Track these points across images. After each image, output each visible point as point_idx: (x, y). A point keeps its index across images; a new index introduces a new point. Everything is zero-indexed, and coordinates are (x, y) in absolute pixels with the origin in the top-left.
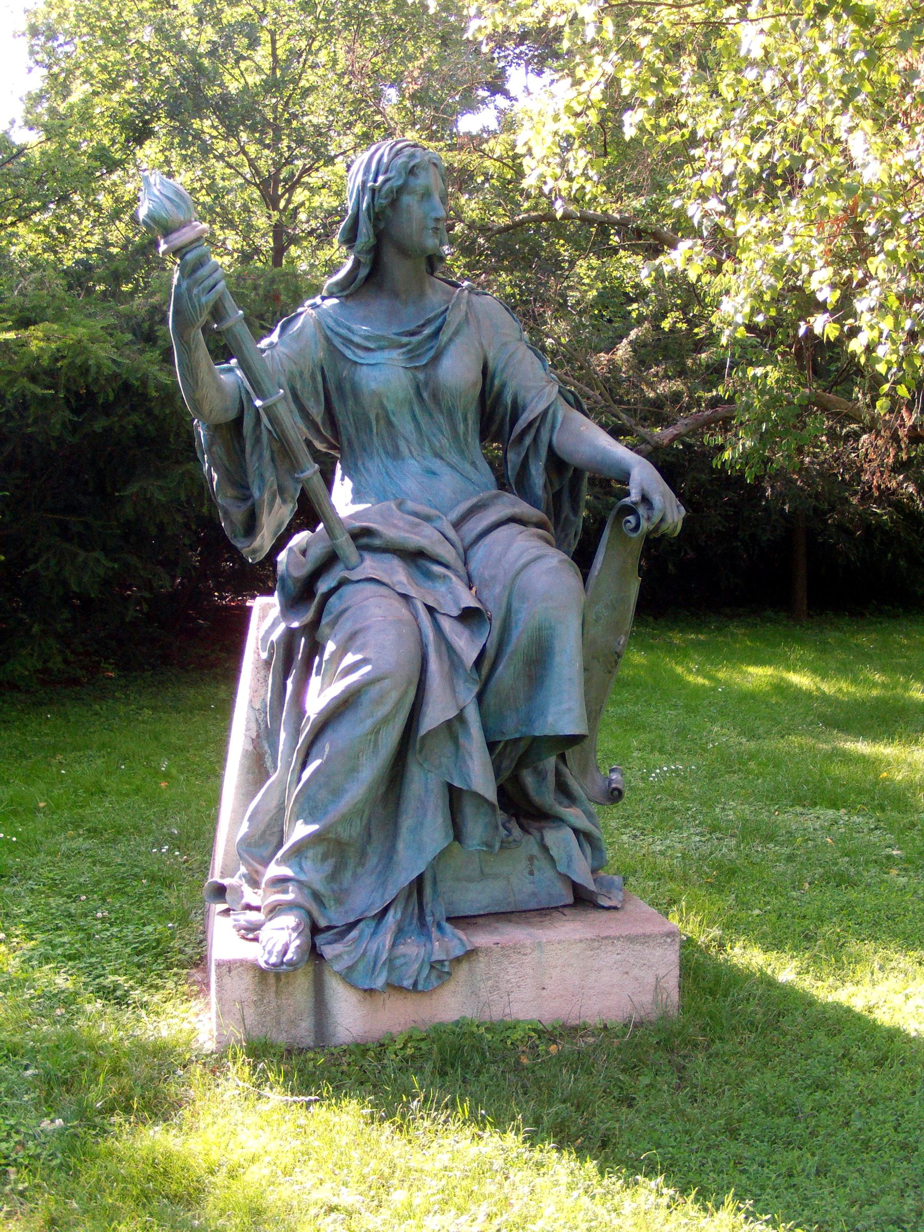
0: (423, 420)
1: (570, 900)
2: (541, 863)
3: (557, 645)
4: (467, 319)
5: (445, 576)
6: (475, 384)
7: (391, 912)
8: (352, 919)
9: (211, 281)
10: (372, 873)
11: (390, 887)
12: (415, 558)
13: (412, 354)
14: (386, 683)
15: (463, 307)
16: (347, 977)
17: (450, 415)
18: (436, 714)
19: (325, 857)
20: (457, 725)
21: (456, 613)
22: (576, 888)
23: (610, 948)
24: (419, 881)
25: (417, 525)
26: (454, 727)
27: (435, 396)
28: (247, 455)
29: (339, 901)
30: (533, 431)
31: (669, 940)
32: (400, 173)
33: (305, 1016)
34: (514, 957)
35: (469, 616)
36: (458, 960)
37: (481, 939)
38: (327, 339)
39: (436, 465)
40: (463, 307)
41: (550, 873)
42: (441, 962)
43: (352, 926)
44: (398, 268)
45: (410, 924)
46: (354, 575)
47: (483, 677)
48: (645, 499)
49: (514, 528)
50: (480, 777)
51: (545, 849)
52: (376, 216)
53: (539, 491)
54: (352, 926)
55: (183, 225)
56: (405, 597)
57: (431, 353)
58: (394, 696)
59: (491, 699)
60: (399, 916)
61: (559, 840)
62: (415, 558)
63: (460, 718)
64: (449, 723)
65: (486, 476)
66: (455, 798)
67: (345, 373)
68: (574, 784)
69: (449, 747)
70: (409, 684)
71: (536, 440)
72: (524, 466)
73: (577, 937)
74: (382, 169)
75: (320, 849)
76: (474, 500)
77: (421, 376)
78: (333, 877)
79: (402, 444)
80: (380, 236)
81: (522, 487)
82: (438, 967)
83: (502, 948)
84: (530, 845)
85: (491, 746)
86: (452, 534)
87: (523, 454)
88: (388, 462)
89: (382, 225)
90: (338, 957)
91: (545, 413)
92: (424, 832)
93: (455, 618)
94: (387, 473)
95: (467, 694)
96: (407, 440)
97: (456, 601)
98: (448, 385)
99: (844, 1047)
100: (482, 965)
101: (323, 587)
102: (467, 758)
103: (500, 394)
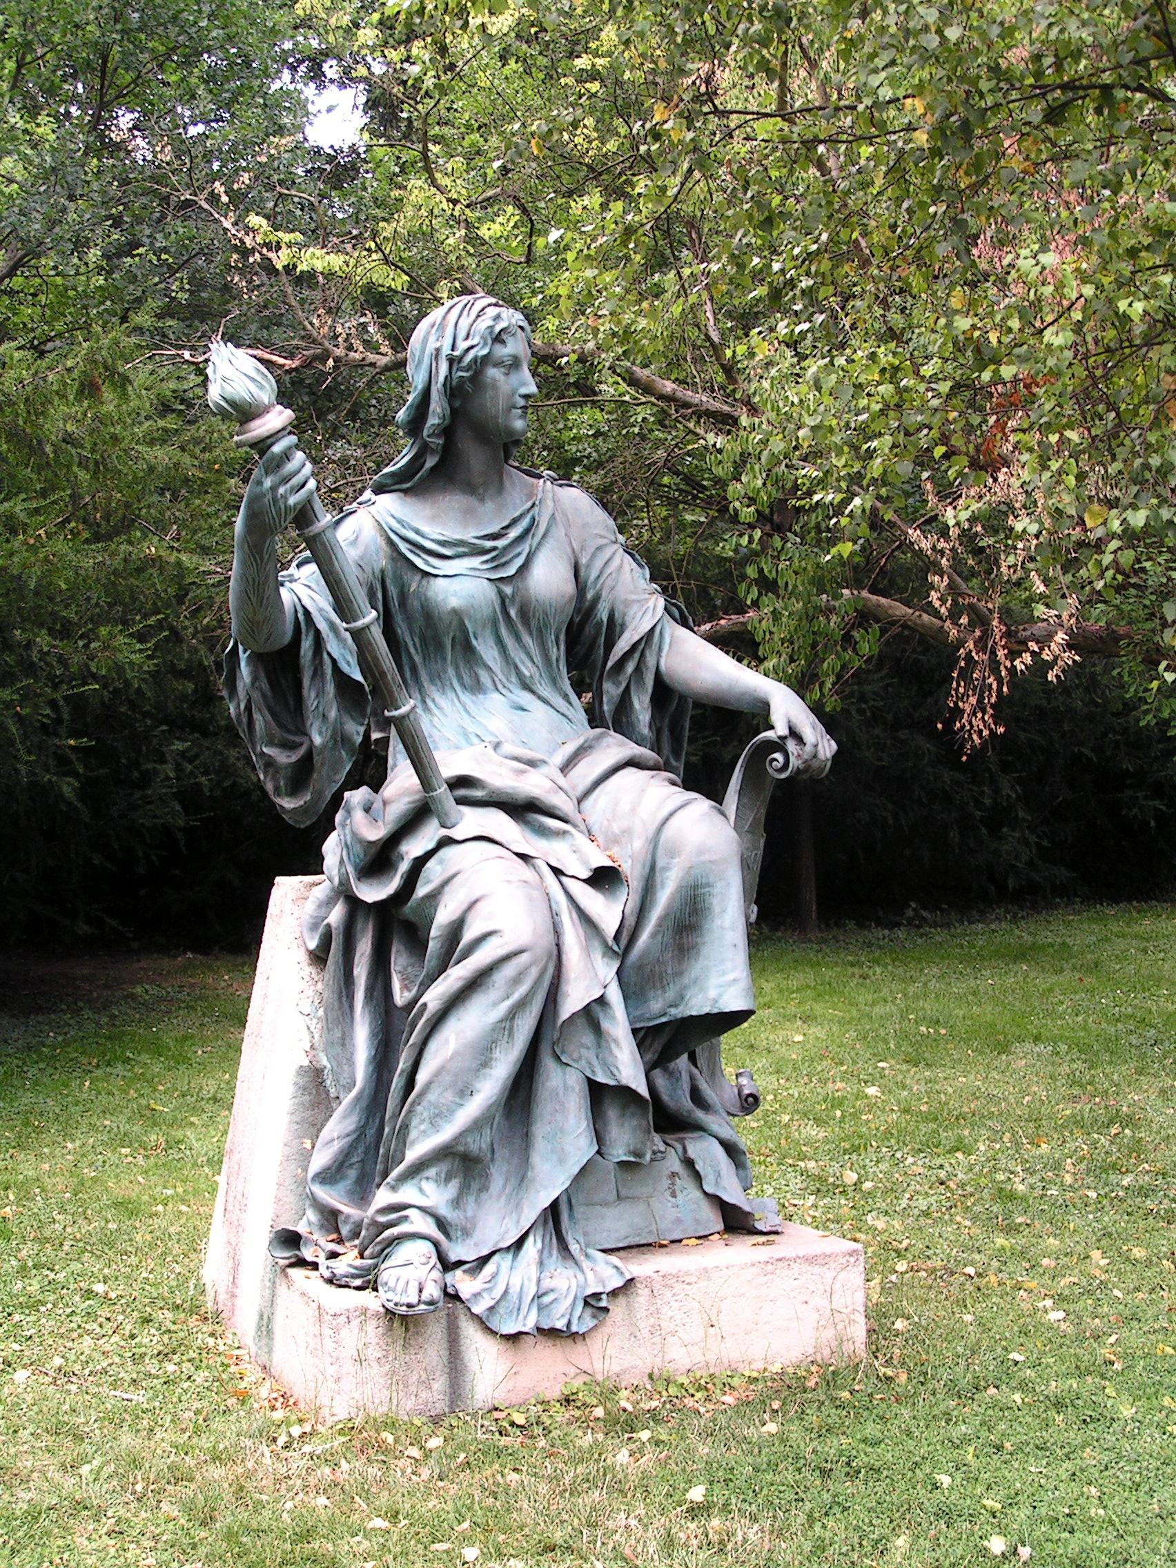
1: (720, 1226)
3: (715, 902)
5: (565, 832)
6: (571, 599)
7: (531, 1239)
8: (485, 1252)
9: (296, 481)
10: (500, 1196)
11: (526, 1210)
12: (523, 809)
13: (498, 559)
14: (524, 958)
15: (550, 503)
18: (573, 1000)
19: (448, 1179)
20: (596, 1008)
21: (585, 874)
23: (786, 1272)
24: (554, 1207)
25: (523, 772)
26: (592, 1014)
27: (524, 614)
28: (305, 692)
29: (466, 1233)
30: (637, 655)
31: (852, 1260)
32: (483, 338)
33: (438, 1373)
34: (678, 1287)
35: (604, 878)
36: (614, 1293)
37: (640, 1267)
38: (391, 543)
39: (525, 698)
40: (550, 503)
41: (689, 1194)
42: (597, 1296)
43: (484, 1260)
44: (475, 457)
45: (551, 1255)
46: (457, 833)
47: (622, 947)
48: (794, 734)
49: (630, 771)
51: (689, 1163)
52: (454, 391)
53: (646, 731)
54: (484, 1260)
56: (523, 857)
57: (519, 562)
60: (539, 1244)
61: (706, 1152)
62: (523, 809)
63: (602, 1001)
64: (587, 1009)
66: (598, 1094)
67: (413, 587)
69: (588, 1038)
70: (550, 957)
71: (638, 670)
72: (624, 703)
74: (462, 334)
75: (444, 1167)
76: (570, 748)
77: (508, 590)
78: (456, 1203)
79: (484, 677)
81: (621, 722)
82: (593, 1303)
83: (664, 1276)
85: (635, 1032)
87: (624, 685)
88: (466, 698)
89: (457, 404)
90: (477, 1295)
91: (652, 630)
92: (565, 1141)
93: (585, 881)
94: (466, 711)
95: (607, 970)
96: (489, 669)
98: (541, 598)
100: (641, 1299)
101: (413, 848)
102: (613, 1045)
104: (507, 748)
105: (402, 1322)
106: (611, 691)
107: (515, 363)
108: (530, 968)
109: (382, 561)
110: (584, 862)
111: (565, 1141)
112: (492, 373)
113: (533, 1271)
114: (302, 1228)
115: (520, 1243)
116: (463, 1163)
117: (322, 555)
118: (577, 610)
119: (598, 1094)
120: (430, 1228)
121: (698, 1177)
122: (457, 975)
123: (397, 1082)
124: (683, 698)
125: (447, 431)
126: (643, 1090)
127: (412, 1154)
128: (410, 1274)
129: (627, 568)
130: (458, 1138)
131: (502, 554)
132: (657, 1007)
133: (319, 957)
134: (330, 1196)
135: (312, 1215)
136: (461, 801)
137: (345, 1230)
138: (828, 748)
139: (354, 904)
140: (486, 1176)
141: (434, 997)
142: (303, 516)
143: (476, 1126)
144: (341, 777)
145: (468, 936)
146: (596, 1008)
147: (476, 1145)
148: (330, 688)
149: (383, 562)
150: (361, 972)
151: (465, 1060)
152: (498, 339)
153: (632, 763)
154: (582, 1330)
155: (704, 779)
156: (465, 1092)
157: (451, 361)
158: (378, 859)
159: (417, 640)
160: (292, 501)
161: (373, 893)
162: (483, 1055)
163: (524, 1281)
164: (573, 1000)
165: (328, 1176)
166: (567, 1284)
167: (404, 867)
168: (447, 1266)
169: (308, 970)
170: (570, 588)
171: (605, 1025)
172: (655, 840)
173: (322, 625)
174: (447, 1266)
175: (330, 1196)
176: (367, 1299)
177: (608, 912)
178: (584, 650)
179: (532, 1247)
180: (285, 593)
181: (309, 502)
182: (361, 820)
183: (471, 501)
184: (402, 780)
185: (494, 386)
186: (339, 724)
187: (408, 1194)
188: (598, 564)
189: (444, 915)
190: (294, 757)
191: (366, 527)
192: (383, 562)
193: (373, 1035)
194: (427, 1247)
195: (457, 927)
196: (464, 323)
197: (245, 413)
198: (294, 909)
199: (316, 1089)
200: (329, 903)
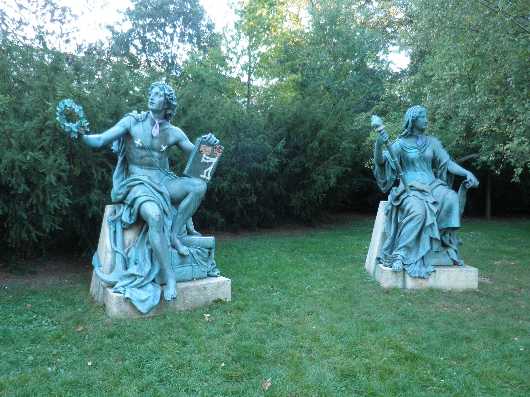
0: (421, 163)
2: (447, 255)
4: (430, 143)
12: (422, 191)
16: (409, 275)
17: (427, 162)
18: (428, 223)
20: (432, 225)
21: (432, 202)
22: (454, 261)
24: (423, 257)
29: (408, 260)
35: (435, 203)
37: (437, 269)
39: (424, 173)
41: (449, 258)
44: (416, 133)
46: (410, 195)
48: (471, 180)
51: (448, 252)
52: (413, 121)
54: (410, 265)
55: (380, 126)
58: (421, 218)
59: (439, 220)
62: (422, 191)
63: (433, 224)
65: (433, 176)
66: (431, 239)
68: (452, 240)
69: (430, 230)
71: (444, 169)
72: (441, 174)
73: (307, 383)
76: (431, 182)
77: (421, 155)
78: (406, 255)
81: (441, 177)
85: (439, 229)
88: (413, 172)
91: (446, 163)
92: (425, 246)
95: (435, 219)
97: (431, 200)
99: (464, 379)
101: (402, 197)
104: (420, 181)
105: (395, 272)
107: (424, 117)
108: (420, 218)
109: (400, 150)
110: (431, 200)
111: (425, 246)
112: (420, 119)
113: (418, 267)
114: (381, 257)
115: (416, 262)
116: (407, 248)
117: (389, 148)
118: (434, 158)
119: (431, 239)
121: (449, 255)
122: (408, 218)
123: (398, 235)
124: (452, 174)
125: (412, 128)
126: (439, 239)
127: (399, 246)
128: (398, 265)
130: (407, 244)
131: (422, 148)
132: (443, 226)
133: (387, 214)
134: (385, 252)
135: (383, 256)
136: (411, 190)
137: (388, 258)
138: (477, 183)
139: (393, 206)
140: (412, 251)
141: (404, 221)
142: (386, 143)
143: (410, 242)
144: (392, 185)
145: (411, 211)
146: (432, 225)
147: (411, 245)
148: (390, 170)
150: (393, 217)
151: (409, 233)
152: (421, 113)
153: (442, 184)
155: (455, 188)
156: (408, 237)
157: (413, 117)
158: (397, 198)
159: (405, 162)
160: (384, 140)
161: (396, 204)
162: (412, 231)
163: (415, 269)
164: (428, 223)
165: (386, 249)
166: (424, 270)
167: (401, 200)
168: (404, 265)
169: (385, 216)
170: (432, 155)
171: (434, 228)
172: (444, 197)
173: (389, 160)
174: (404, 265)
175: (385, 252)
176: (390, 269)
178: (434, 163)
179: (418, 263)
180: (383, 155)
182: (395, 192)
184: (401, 187)
185: (420, 121)
186: (391, 176)
187: (398, 253)
188: (438, 150)
189: (407, 208)
191: (397, 144)
193: (395, 227)
194: (401, 261)
195: (409, 210)
196: (415, 110)
197: (377, 126)
198: (383, 206)
199: (384, 235)
200: (388, 206)
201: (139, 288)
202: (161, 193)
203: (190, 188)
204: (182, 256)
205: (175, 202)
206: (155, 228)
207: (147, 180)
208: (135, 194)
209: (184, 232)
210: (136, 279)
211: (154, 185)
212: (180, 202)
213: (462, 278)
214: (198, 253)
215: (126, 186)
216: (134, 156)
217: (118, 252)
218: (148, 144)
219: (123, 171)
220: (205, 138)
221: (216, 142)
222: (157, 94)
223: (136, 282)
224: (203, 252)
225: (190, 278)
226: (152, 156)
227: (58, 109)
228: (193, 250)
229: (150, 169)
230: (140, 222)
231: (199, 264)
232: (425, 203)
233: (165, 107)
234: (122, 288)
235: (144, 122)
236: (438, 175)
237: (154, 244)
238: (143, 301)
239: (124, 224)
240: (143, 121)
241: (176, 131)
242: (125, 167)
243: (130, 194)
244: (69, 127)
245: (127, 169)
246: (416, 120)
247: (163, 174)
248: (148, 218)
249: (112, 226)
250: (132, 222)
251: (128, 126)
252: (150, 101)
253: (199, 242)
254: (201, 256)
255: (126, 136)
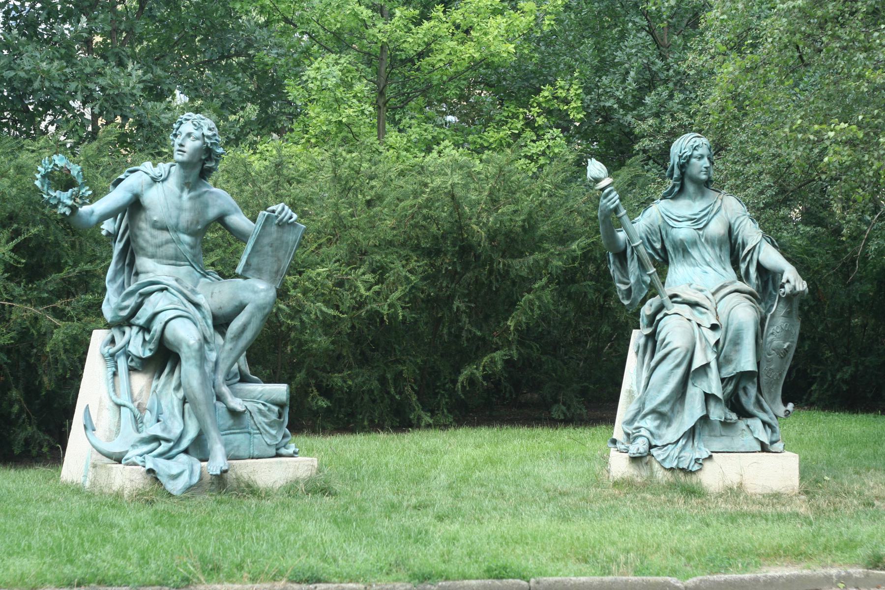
0: (703, 250)
2: (747, 432)
3: (745, 336)
12: (694, 305)
18: (696, 365)
22: (762, 444)
26: (705, 367)
35: (714, 327)
39: (708, 269)
41: (752, 437)
42: (698, 459)
43: (664, 446)
50: (715, 388)
56: (689, 320)
58: (682, 355)
62: (694, 305)
63: (707, 365)
70: (687, 351)
75: (654, 416)
77: (701, 232)
78: (658, 427)
80: (683, 174)
84: (742, 424)
86: (710, 296)
90: (659, 455)
91: (754, 247)
92: (693, 410)
95: (712, 357)
101: (658, 317)
103: (736, 239)
106: (743, 266)
112: (693, 160)
120: (648, 434)
121: (752, 432)
129: (748, 225)
143: (663, 403)
147: (665, 409)
149: (660, 222)
154: (693, 470)
156: (659, 391)
157: (680, 157)
160: (612, 207)
171: (710, 375)
177: (712, 337)
178: (733, 249)
181: (617, 206)
183: (690, 202)
190: (627, 287)
192: (660, 222)
195: (664, 340)
197: (597, 180)
201: (169, 458)
202: (197, 305)
203: (246, 296)
204: (234, 414)
205: (221, 323)
206: (192, 361)
207: (173, 283)
208: (155, 307)
209: (235, 376)
210: (160, 444)
211: (186, 291)
212: (231, 321)
213: (776, 471)
214: (260, 410)
215: (137, 294)
216: (147, 241)
217: (124, 406)
218: (172, 222)
219: (122, 269)
220: (274, 212)
221: (291, 218)
222: (189, 135)
223: (160, 450)
224: (269, 410)
225: (246, 454)
226: (180, 241)
227: (40, 168)
228: (250, 406)
229: (176, 265)
230: (163, 358)
231: (262, 430)
232: (696, 327)
233: (203, 157)
234: (139, 458)
235: (166, 183)
236: (742, 272)
237: (191, 387)
238: (175, 477)
239: (132, 360)
240: (163, 181)
241: (219, 196)
242: (127, 262)
243: (141, 310)
244: (55, 197)
245: (132, 263)
246: (688, 162)
247: (198, 275)
248: (180, 344)
249: (111, 363)
250: (148, 354)
251: (138, 190)
252: (177, 147)
253: (261, 392)
254: (265, 416)
255: (135, 207)
